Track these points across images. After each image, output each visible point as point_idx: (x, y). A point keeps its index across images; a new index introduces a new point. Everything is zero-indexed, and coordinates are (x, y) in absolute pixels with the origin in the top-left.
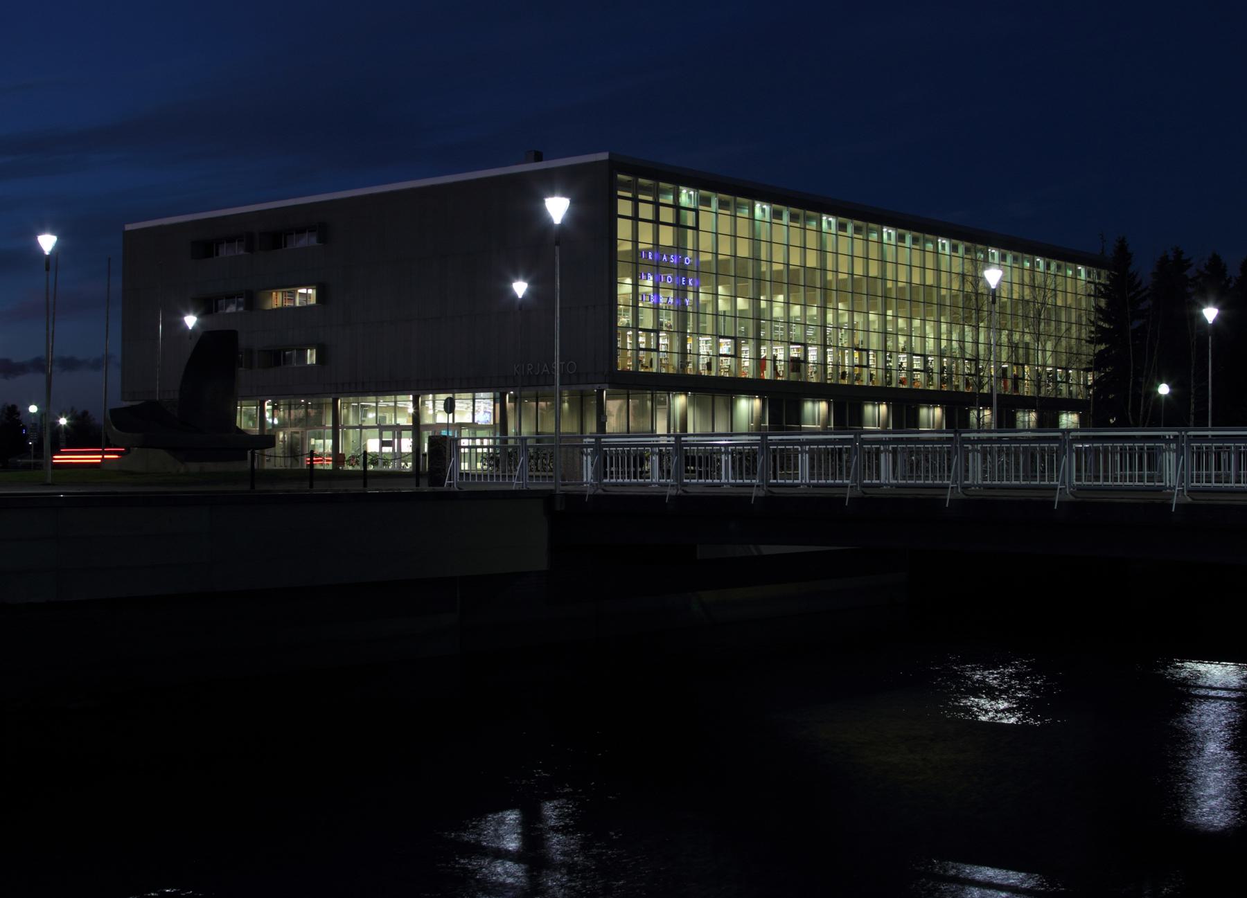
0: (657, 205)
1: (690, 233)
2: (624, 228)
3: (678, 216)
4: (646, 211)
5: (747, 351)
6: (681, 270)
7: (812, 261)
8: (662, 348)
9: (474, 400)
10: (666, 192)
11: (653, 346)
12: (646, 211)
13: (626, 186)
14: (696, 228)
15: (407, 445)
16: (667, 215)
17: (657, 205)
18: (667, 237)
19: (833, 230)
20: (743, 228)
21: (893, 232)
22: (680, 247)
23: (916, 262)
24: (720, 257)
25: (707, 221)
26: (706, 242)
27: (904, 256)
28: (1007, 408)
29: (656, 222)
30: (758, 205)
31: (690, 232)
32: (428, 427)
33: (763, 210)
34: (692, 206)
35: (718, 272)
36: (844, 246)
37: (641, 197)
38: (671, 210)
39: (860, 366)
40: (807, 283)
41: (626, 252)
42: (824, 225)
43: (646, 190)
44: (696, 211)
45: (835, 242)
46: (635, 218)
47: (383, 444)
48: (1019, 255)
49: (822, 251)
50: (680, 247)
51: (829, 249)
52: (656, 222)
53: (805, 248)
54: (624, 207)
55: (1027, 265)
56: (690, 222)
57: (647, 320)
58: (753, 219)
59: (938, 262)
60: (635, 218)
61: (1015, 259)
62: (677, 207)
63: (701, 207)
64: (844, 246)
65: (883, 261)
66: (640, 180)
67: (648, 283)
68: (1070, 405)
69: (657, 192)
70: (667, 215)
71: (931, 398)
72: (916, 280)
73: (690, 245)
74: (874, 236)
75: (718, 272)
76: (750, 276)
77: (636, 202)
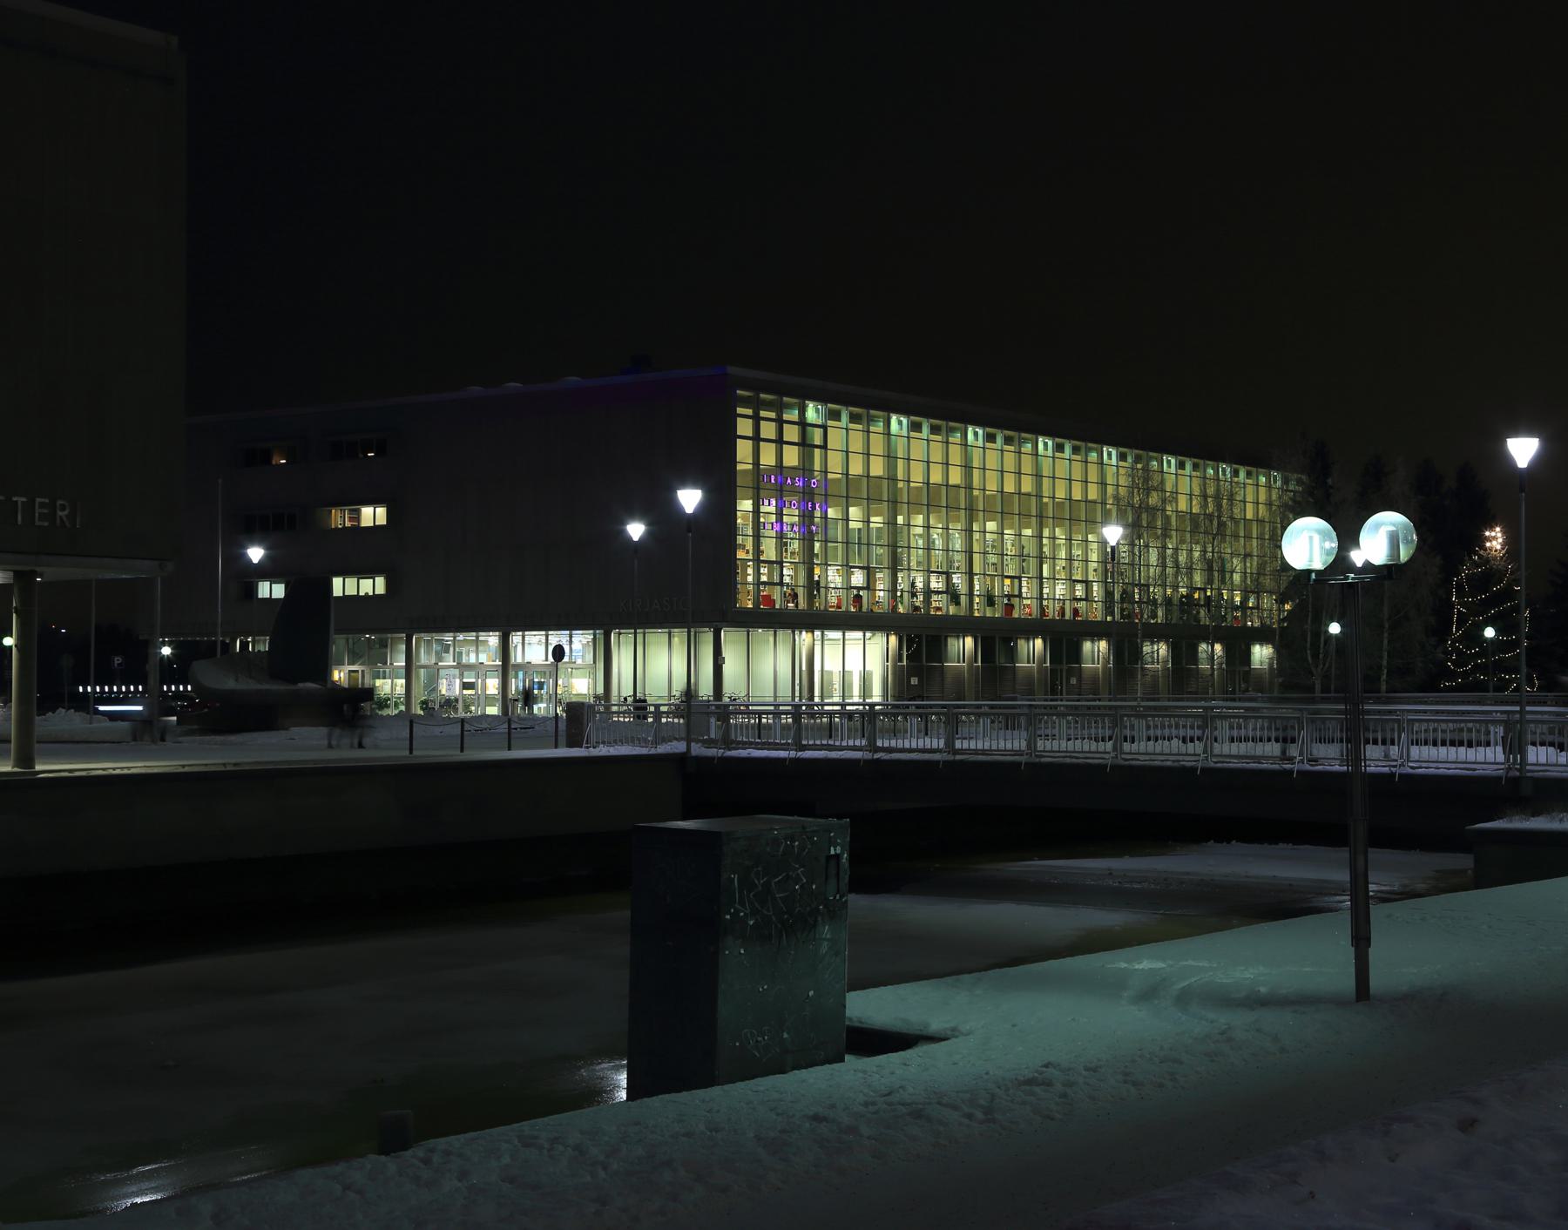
0: (780, 422)
1: (817, 451)
2: (744, 450)
3: (803, 434)
4: (768, 430)
5: (882, 583)
6: (803, 488)
7: (956, 477)
8: (787, 580)
9: (775, 696)
10: (790, 407)
11: (776, 579)
12: (768, 430)
13: (746, 402)
14: (824, 447)
15: (493, 686)
16: (791, 433)
17: (780, 422)
18: (791, 457)
19: (980, 443)
20: (956, 455)
21: (980, 432)
22: (805, 469)
23: (1077, 475)
24: (830, 476)
25: (836, 438)
26: (835, 462)
27: (1062, 469)
28: (1184, 639)
29: (780, 441)
30: (894, 419)
31: (817, 451)
32: (518, 667)
33: (900, 423)
34: (820, 422)
35: (851, 490)
36: (992, 460)
37: (763, 414)
38: (796, 427)
39: (1009, 596)
40: (960, 503)
41: (745, 471)
42: (1041, 446)
43: (768, 406)
44: (824, 427)
45: (985, 457)
46: (756, 438)
47: (466, 686)
48: (1201, 462)
49: (1038, 476)
50: (805, 469)
51: (975, 464)
52: (780, 441)
53: (868, 454)
54: (744, 427)
55: (1263, 479)
56: (818, 441)
57: (769, 550)
58: (889, 434)
59: (1102, 474)
60: (756, 438)
61: (1195, 467)
62: (803, 424)
63: (830, 423)
64: (992, 460)
65: (1038, 476)
66: (762, 396)
67: (769, 507)
68: (1263, 635)
69: (780, 408)
70: (791, 433)
71: (1095, 631)
72: (1077, 495)
73: (817, 466)
74: (1028, 447)
75: (851, 490)
76: (885, 494)
77: (757, 419)
